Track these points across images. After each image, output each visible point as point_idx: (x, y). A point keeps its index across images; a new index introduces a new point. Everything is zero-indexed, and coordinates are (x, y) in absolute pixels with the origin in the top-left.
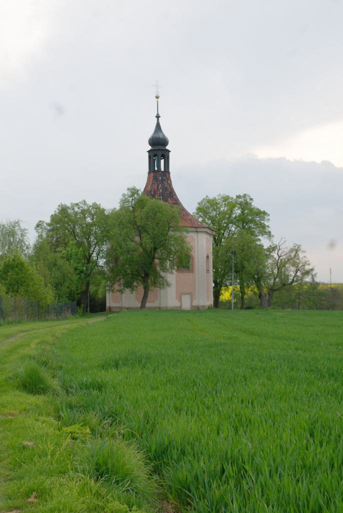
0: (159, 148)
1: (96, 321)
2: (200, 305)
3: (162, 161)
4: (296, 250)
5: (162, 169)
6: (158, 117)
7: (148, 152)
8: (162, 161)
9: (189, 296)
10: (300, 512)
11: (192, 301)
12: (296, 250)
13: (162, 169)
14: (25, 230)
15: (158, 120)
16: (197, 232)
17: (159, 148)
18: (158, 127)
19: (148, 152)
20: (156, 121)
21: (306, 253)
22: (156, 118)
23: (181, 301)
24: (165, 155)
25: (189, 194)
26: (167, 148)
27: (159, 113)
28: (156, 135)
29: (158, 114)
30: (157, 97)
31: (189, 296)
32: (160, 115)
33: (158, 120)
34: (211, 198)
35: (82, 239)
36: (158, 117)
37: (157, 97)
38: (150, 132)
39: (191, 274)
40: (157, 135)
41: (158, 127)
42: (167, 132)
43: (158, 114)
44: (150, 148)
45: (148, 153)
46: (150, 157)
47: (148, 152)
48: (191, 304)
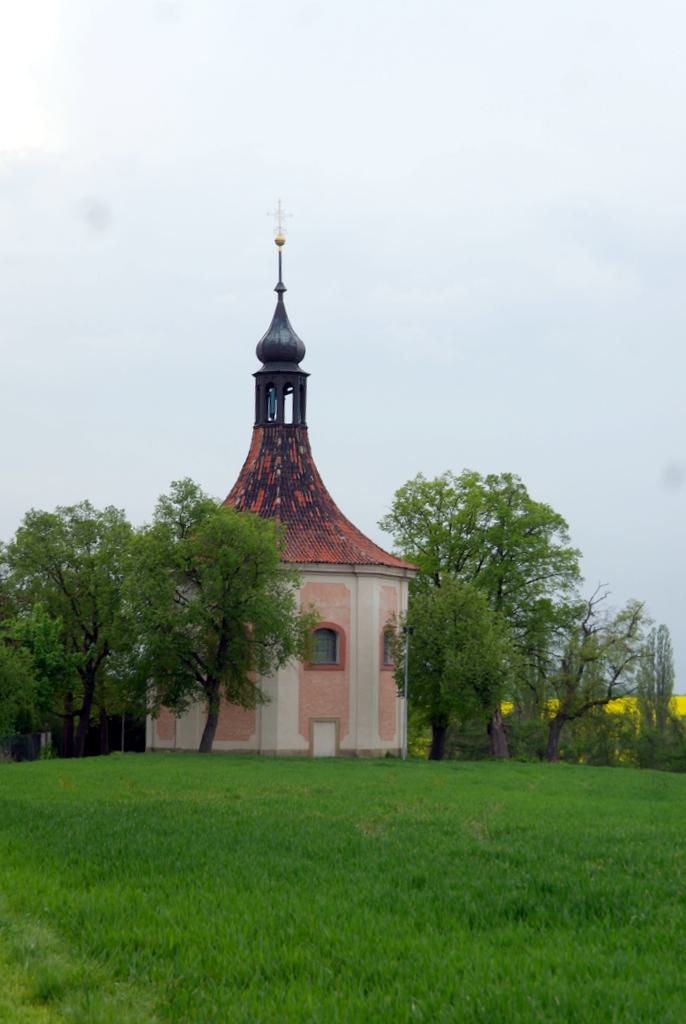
0: (280, 368)
4: (307, 375)
5: (288, 419)
6: (280, 290)
7: (255, 375)
8: (289, 399)
9: (331, 727)
12: (307, 375)
13: (288, 419)
15: (280, 298)
17: (280, 368)
18: (280, 315)
19: (255, 375)
20: (276, 301)
22: (277, 294)
23: (310, 738)
24: (297, 383)
26: (303, 366)
27: (283, 281)
28: (272, 337)
29: (280, 284)
30: (280, 243)
31: (331, 727)
32: (286, 285)
33: (280, 298)
36: (280, 290)
37: (280, 243)
38: (260, 327)
39: (338, 675)
40: (275, 338)
41: (280, 315)
42: (301, 327)
43: (280, 284)
44: (259, 366)
45: (254, 379)
48: (337, 745)
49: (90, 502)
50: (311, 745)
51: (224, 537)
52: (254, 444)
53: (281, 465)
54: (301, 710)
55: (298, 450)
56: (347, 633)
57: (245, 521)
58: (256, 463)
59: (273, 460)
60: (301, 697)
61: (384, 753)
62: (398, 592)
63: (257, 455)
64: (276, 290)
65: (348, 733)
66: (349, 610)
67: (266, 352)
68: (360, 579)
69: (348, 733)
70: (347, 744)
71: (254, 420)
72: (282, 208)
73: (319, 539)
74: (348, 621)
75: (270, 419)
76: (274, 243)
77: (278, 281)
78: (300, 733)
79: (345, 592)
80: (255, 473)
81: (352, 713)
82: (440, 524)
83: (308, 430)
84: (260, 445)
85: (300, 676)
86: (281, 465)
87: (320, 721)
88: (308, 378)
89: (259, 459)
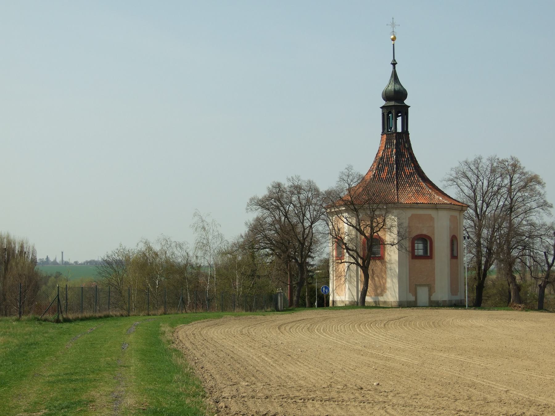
0: (396, 104)
3: (399, 120)
6: (394, 64)
7: (381, 108)
8: (399, 120)
11: (430, 295)
13: (399, 130)
14: (539, 183)
15: (394, 68)
17: (396, 104)
19: (381, 108)
22: (234, 224)
23: (415, 294)
24: (403, 111)
26: (406, 102)
29: (394, 60)
33: (394, 68)
34: (12, 237)
36: (394, 64)
38: (384, 83)
44: (383, 103)
46: (383, 114)
48: (430, 298)
54: (410, 280)
55: (405, 146)
59: (392, 151)
67: (387, 97)
70: (435, 298)
71: (381, 131)
73: (417, 191)
79: (432, 219)
80: (382, 158)
87: (420, 285)
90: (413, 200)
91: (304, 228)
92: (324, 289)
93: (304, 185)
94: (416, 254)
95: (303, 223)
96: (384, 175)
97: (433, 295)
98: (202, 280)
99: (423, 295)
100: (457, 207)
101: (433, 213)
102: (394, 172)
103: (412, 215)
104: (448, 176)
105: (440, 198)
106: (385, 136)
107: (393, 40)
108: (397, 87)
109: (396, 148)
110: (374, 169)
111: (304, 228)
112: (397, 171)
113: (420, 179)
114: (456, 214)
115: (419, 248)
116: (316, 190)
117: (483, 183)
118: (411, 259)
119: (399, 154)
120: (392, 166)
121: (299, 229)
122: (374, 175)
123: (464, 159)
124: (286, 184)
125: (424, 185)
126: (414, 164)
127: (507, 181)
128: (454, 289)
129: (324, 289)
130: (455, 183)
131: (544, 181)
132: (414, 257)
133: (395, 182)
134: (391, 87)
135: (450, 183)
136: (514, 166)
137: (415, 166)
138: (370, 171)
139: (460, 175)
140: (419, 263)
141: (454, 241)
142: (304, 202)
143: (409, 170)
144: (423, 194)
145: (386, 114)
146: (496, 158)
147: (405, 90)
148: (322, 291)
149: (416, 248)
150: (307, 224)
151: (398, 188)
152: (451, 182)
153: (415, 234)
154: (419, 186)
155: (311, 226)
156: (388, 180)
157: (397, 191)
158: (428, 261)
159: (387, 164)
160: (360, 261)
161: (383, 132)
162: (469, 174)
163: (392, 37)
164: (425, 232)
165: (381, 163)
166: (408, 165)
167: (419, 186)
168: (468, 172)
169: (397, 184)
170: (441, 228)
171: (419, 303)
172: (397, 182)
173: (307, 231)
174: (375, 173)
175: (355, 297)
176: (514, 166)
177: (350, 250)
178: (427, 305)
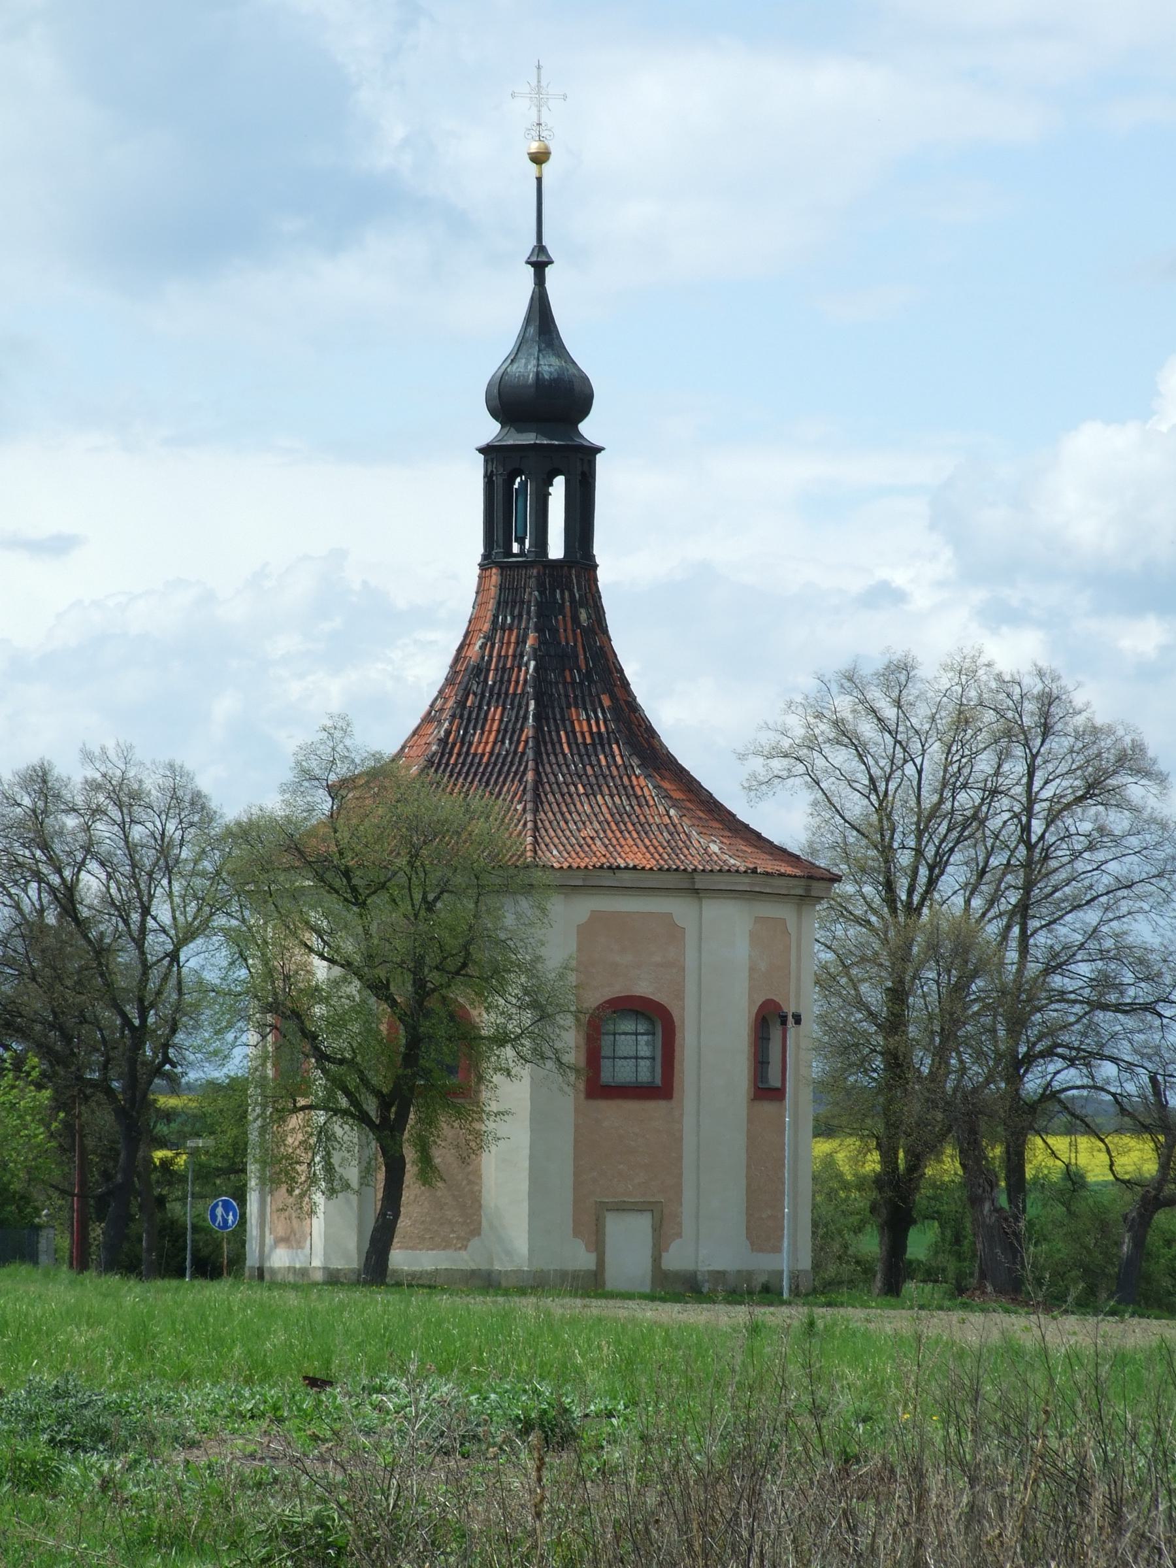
0: (541, 428)
1: (215, 1292)
2: (704, 1268)
4: (599, 450)
5: (556, 549)
6: (540, 264)
7: (481, 450)
9: (642, 1224)
10: (1073, 1556)
12: (599, 450)
13: (556, 549)
16: (695, 892)
17: (541, 428)
18: (541, 320)
19: (481, 450)
21: (107, 746)
23: (598, 1246)
24: (580, 465)
25: (712, 697)
26: (590, 429)
29: (540, 248)
30: (539, 158)
31: (642, 1224)
35: (69, 864)
36: (540, 264)
38: (490, 336)
41: (541, 320)
42: (585, 344)
44: (490, 430)
47: (485, 450)
48: (656, 1260)
49: (178, 763)
50: (601, 1262)
51: (420, 838)
52: (478, 604)
53: (545, 654)
54: (578, 1185)
55: (575, 619)
56: (677, 1030)
57: (447, 803)
58: (483, 647)
59: (521, 641)
60: (576, 1158)
61: (763, 1279)
62: (792, 929)
63: (486, 627)
64: (528, 263)
65: (680, 1235)
66: (683, 969)
67: (507, 402)
68: (705, 902)
69: (680, 1235)
70: (677, 1259)
71: (479, 549)
72: (534, 110)
73: (619, 815)
74: (680, 995)
75: (516, 548)
76: (527, 158)
77: (533, 242)
78: (577, 1233)
79: (675, 933)
80: (479, 671)
81: (688, 1195)
82: (67, 899)
83: (599, 572)
84: (492, 605)
85: (577, 1110)
86: (545, 654)
87: (621, 1208)
88: (598, 456)
89: (490, 638)
90: (599, 854)
91: (144, 962)
92: (220, 1211)
93: (152, 783)
94: (606, 1077)
95: (140, 943)
96: (483, 743)
97: (674, 1246)
98: (700, 1277)
99: (629, 1246)
100: (781, 882)
101: (679, 909)
102: (529, 732)
103: (596, 916)
104: (767, 739)
105: (714, 848)
106: (495, 576)
107: (539, 158)
108: (550, 366)
109: (539, 629)
110: (446, 715)
111: (144, 962)
112: (538, 729)
113: (635, 762)
114: (784, 912)
115: (632, 1050)
116: (198, 802)
117: (920, 772)
118: (582, 1096)
119: (552, 657)
120: (521, 706)
121: (126, 957)
122: (443, 742)
123: (843, 664)
124: (72, 773)
125: (646, 786)
126: (613, 697)
127: (1016, 768)
128: (762, 1229)
129: (220, 1211)
130: (800, 768)
131: (1162, 766)
132: (598, 1088)
133: (530, 776)
134: (527, 369)
135: (778, 764)
136: (1048, 701)
137: (616, 709)
138: (428, 719)
139: (824, 729)
140: (615, 1115)
141: (770, 1021)
142: (148, 858)
143: (584, 723)
144: (643, 828)
145: (498, 481)
146: (983, 660)
147: (585, 380)
148: (214, 1217)
149: (606, 1051)
150: (157, 944)
151: (537, 800)
152: (785, 762)
153: (594, 998)
154: (629, 792)
155: (174, 956)
156: (492, 772)
157: (536, 811)
158: (654, 1108)
159: (499, 695)
160: (371, 1106)
161: (486, 557)
162: (867, 729)
163: (534, 147)
164: (644, 988)
165: (473, 686)
166: (588, 702)
167: (629, 792)
168: (870, 713)
169: (538, 782)
170: (717, 965)
171: (613, 1279)
172: (537, 772)
173: (155, 975)
174: (448, 733)
175: (350, 1257)
176: (1048, 701)
177: (328, 1058)
178: (647, 1289)
